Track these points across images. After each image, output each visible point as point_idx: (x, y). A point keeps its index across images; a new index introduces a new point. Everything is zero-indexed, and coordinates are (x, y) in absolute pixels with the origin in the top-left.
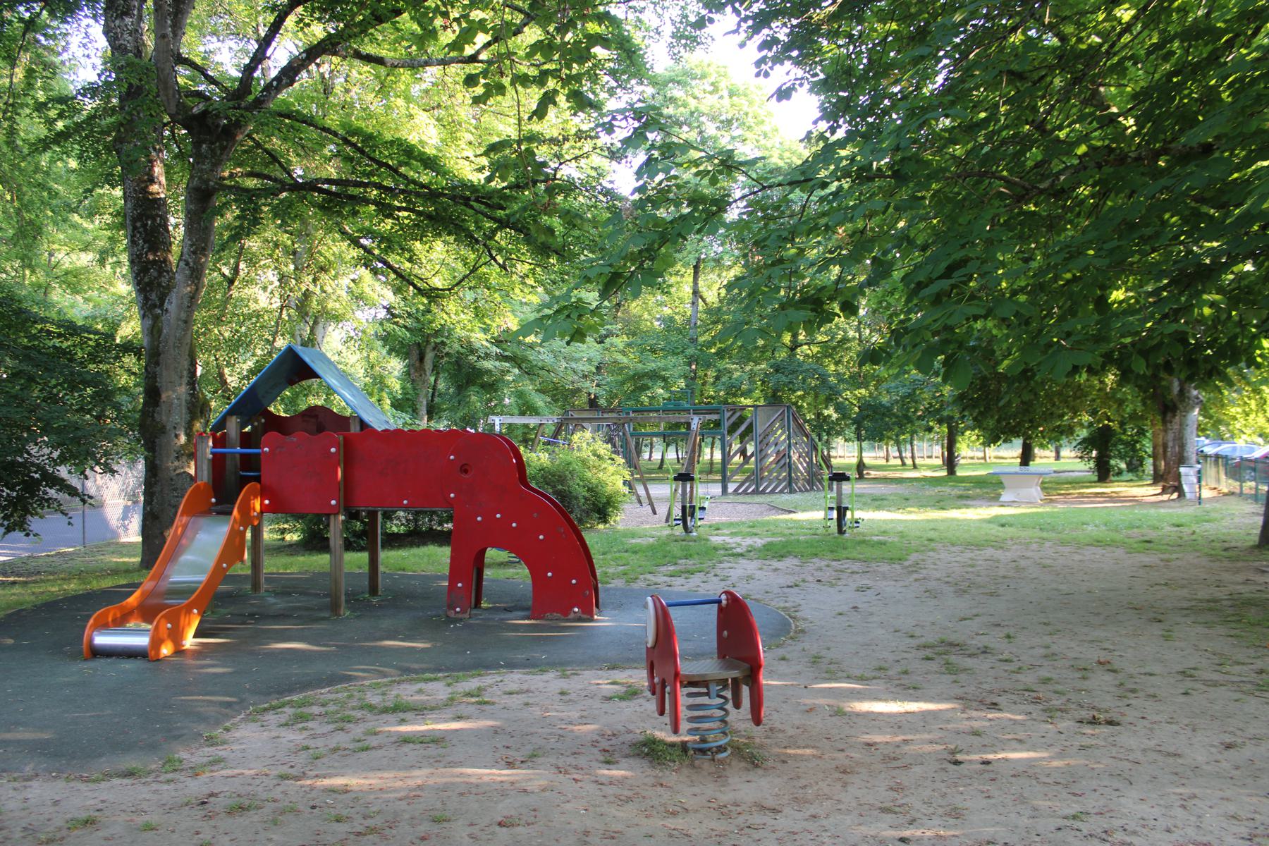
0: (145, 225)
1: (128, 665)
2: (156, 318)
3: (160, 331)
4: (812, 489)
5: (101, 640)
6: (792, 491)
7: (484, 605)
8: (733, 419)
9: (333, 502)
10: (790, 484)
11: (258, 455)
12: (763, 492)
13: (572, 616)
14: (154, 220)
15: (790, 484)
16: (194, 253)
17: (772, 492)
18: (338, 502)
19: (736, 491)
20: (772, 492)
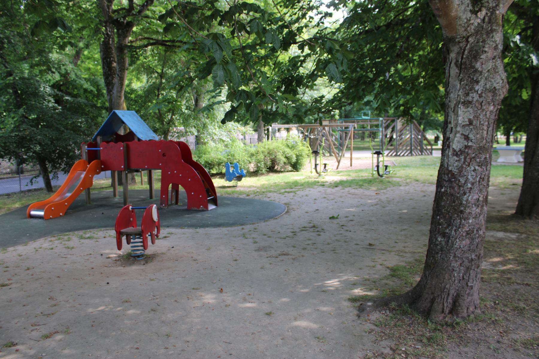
0: (107, 61)
1: (40, 220)
2: (111, 95)
3: (112, 101)
4: (422, 154)
5: (33, 213)
6: (412, 155)
7: (179, 204)
8: (387, 123)
9: (122, 167)
10: (411, 152)
11: (96, 151)
12: (399, 155)
13: (200, 209)
14: (110, 59)
15: (411, 152)
16: (120, 71)
17: (403, 155)
18: (124, 167)
19: (387, 155)
20: (403, 155)
